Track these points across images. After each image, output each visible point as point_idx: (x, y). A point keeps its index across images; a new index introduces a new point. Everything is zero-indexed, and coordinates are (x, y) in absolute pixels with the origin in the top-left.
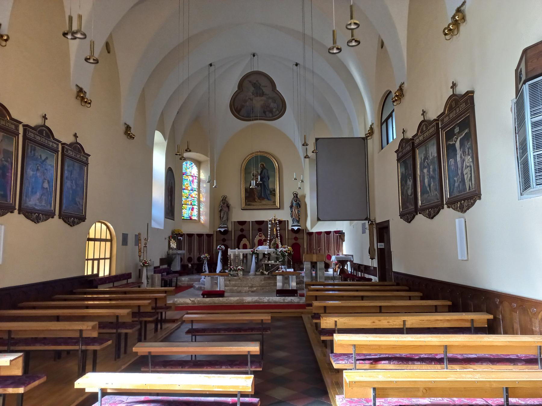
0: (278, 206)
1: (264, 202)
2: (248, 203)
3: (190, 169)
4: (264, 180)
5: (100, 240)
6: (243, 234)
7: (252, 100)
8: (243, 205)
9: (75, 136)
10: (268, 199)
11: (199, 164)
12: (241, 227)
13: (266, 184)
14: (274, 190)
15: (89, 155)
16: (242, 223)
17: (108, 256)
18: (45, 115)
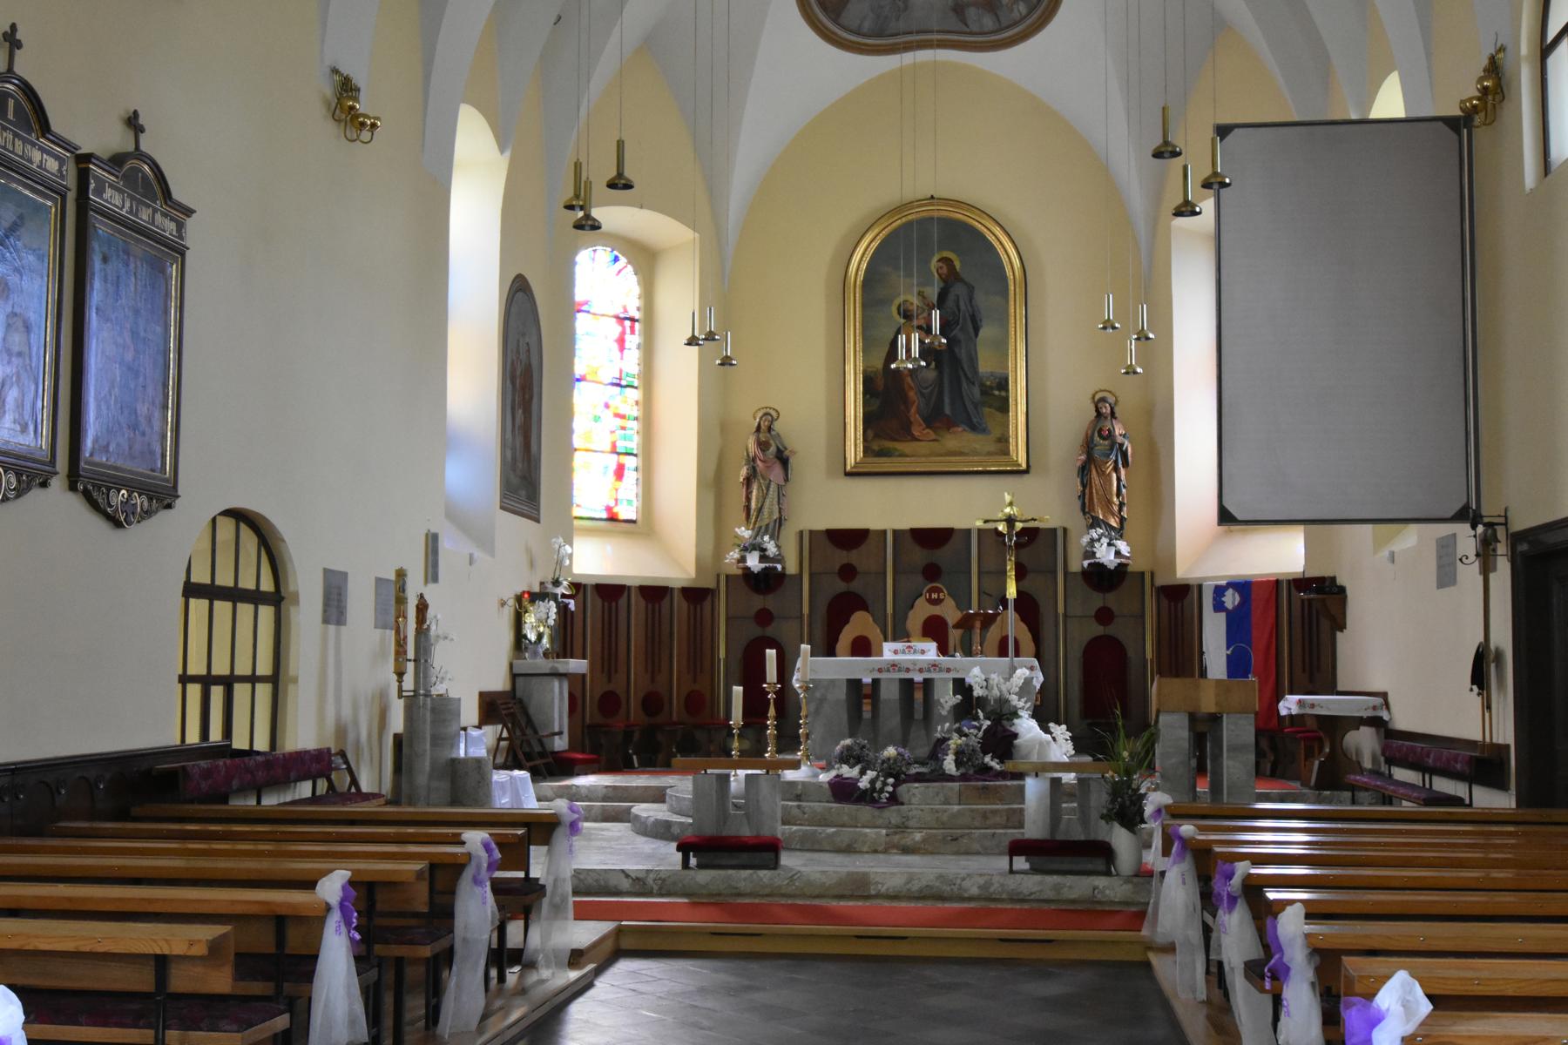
0: (1022, 460)
1: (952, 441)
2: (875, 447)
3: (600, 281)
4: (956, 332)
5: (235, 595)
6: (849, 582)
8: (854, 452)
9: (133, 123)
10: (974, 428)
11: (644, 258)
12: (840, 557)
13: (962, 353)
14: (1003, 384)
15: (189, 212)
17: (264, 668)
18: (13, 27)
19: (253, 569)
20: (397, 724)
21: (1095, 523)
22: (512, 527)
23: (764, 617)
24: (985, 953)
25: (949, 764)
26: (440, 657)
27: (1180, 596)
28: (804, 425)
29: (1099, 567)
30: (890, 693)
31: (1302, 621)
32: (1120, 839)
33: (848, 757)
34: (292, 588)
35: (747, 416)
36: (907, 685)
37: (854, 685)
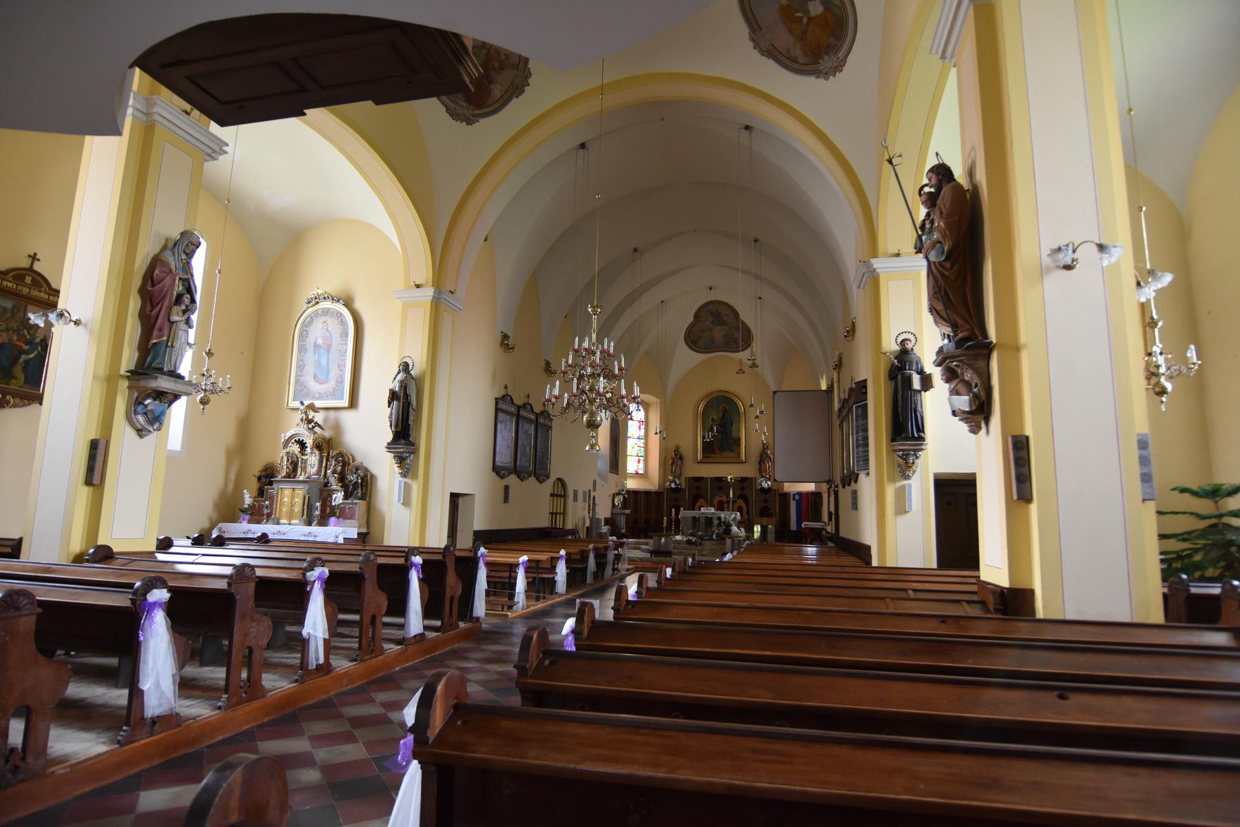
1: (725, 454)
6: (699, 490)
8: (700, 456)
14: (739, 439)
16: (699, 479)
19: (561, 491)
20: (588, 524)
22: (612, 477)
23: (676, 500)
26: (598, 509)
27: (785, 496)
28: (686, 450)
30: (702, 520)
33: (691, 535)
34: (137, 354)
35: (672, 446)
36: (707, 518)
37: (694, 518)
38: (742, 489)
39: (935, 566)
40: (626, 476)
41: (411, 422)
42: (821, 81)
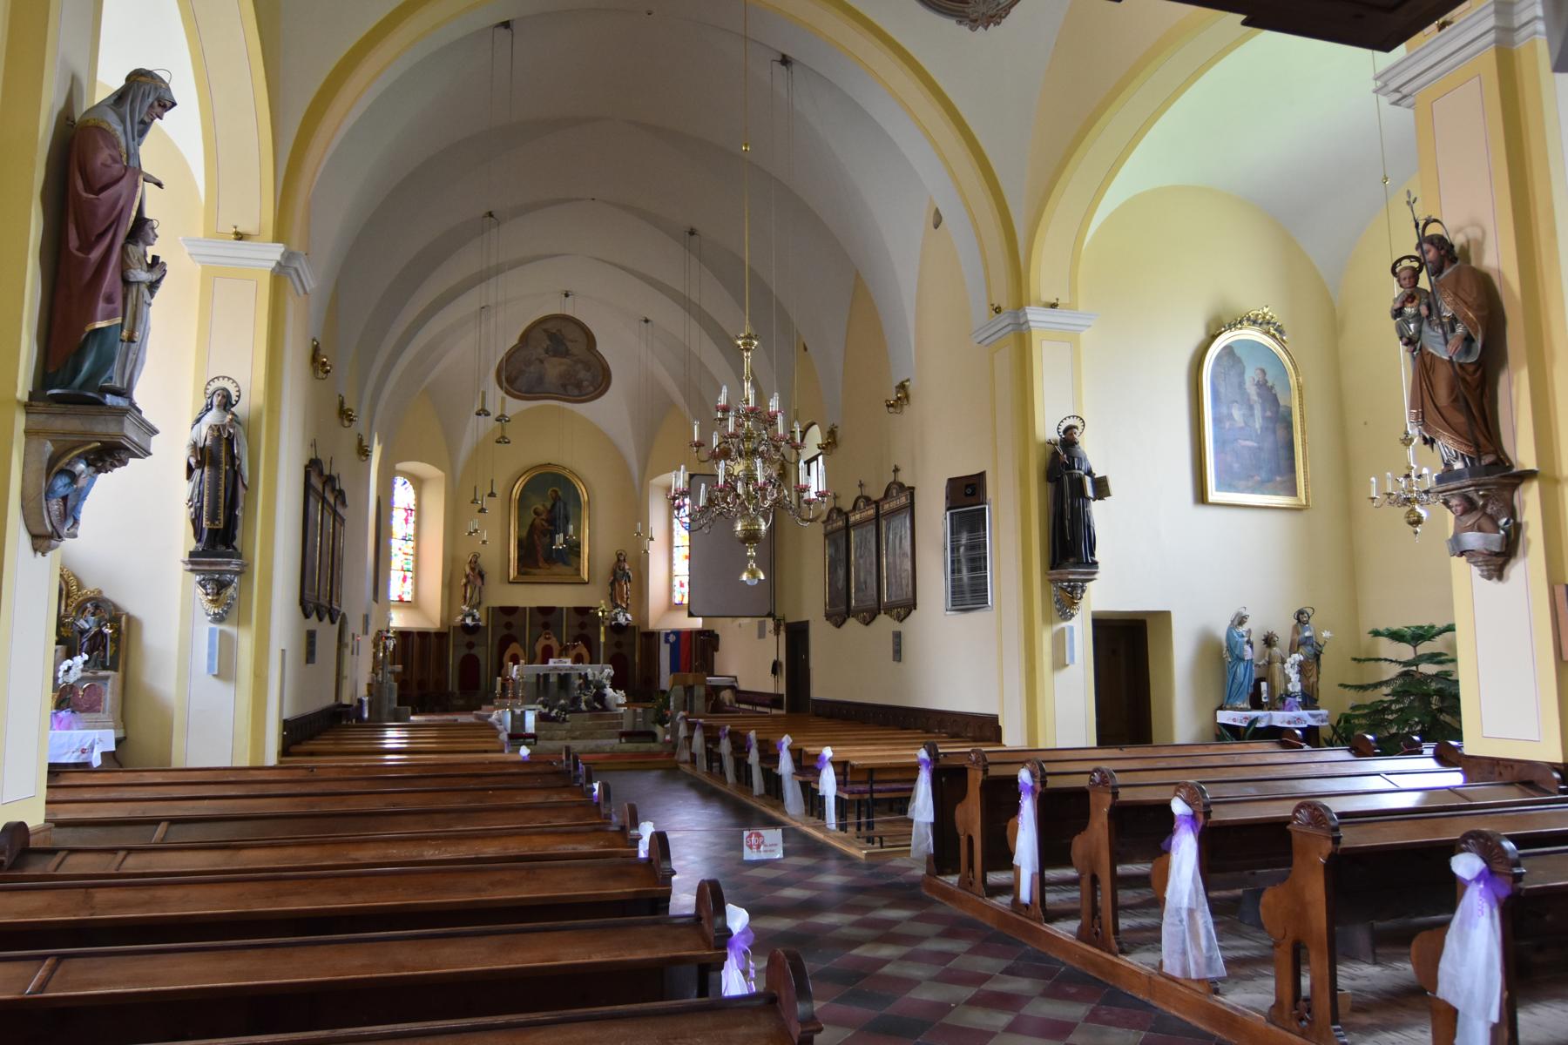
7: (542, 362)
8: (513, 573)
11: (418, 483)
12: (506, 619)
21: (617, 606)
24: (259, 903)
25: (583, 706)
27: (651, 637)
28: (490, 560)
29: (619, 625)
30: (553, 679)
31: (698, 649)
32: (658, 729)
38: (582, 626)
39: (1094, 744)
40: (387, 606)
41: (238, 512)
42: (964, 30)
